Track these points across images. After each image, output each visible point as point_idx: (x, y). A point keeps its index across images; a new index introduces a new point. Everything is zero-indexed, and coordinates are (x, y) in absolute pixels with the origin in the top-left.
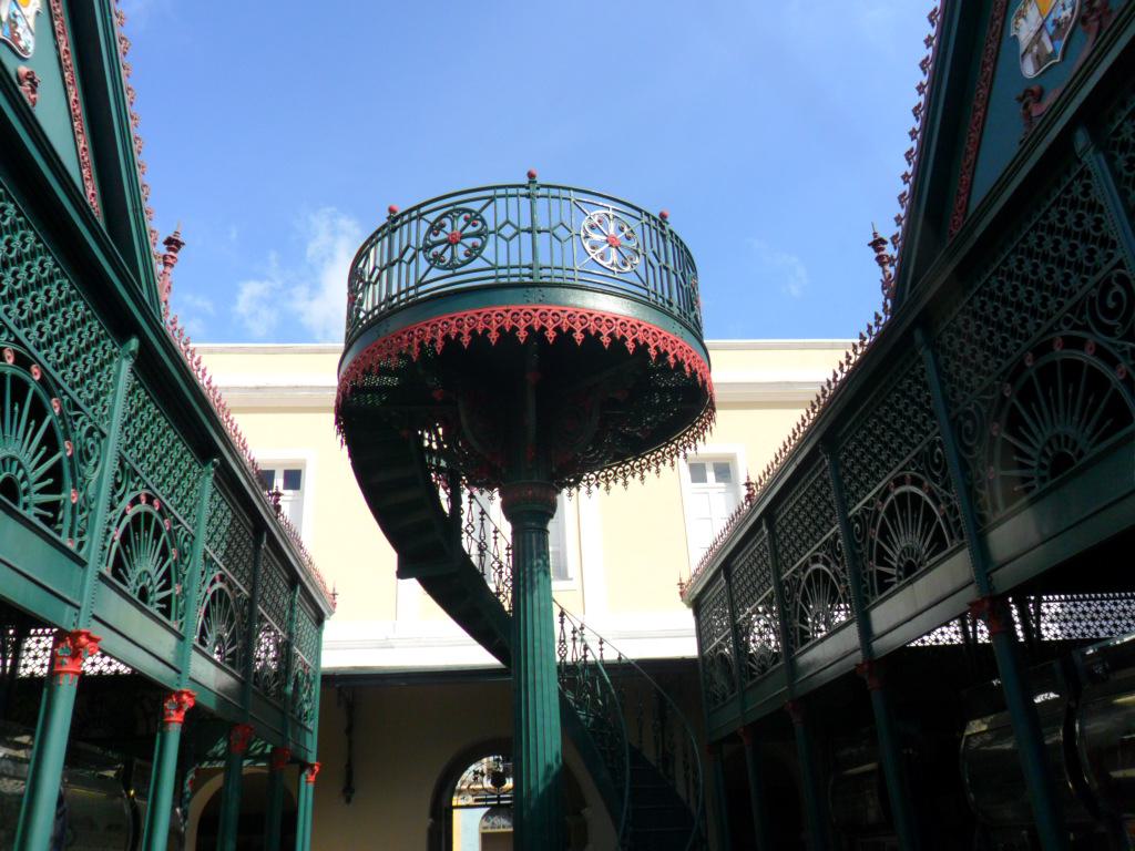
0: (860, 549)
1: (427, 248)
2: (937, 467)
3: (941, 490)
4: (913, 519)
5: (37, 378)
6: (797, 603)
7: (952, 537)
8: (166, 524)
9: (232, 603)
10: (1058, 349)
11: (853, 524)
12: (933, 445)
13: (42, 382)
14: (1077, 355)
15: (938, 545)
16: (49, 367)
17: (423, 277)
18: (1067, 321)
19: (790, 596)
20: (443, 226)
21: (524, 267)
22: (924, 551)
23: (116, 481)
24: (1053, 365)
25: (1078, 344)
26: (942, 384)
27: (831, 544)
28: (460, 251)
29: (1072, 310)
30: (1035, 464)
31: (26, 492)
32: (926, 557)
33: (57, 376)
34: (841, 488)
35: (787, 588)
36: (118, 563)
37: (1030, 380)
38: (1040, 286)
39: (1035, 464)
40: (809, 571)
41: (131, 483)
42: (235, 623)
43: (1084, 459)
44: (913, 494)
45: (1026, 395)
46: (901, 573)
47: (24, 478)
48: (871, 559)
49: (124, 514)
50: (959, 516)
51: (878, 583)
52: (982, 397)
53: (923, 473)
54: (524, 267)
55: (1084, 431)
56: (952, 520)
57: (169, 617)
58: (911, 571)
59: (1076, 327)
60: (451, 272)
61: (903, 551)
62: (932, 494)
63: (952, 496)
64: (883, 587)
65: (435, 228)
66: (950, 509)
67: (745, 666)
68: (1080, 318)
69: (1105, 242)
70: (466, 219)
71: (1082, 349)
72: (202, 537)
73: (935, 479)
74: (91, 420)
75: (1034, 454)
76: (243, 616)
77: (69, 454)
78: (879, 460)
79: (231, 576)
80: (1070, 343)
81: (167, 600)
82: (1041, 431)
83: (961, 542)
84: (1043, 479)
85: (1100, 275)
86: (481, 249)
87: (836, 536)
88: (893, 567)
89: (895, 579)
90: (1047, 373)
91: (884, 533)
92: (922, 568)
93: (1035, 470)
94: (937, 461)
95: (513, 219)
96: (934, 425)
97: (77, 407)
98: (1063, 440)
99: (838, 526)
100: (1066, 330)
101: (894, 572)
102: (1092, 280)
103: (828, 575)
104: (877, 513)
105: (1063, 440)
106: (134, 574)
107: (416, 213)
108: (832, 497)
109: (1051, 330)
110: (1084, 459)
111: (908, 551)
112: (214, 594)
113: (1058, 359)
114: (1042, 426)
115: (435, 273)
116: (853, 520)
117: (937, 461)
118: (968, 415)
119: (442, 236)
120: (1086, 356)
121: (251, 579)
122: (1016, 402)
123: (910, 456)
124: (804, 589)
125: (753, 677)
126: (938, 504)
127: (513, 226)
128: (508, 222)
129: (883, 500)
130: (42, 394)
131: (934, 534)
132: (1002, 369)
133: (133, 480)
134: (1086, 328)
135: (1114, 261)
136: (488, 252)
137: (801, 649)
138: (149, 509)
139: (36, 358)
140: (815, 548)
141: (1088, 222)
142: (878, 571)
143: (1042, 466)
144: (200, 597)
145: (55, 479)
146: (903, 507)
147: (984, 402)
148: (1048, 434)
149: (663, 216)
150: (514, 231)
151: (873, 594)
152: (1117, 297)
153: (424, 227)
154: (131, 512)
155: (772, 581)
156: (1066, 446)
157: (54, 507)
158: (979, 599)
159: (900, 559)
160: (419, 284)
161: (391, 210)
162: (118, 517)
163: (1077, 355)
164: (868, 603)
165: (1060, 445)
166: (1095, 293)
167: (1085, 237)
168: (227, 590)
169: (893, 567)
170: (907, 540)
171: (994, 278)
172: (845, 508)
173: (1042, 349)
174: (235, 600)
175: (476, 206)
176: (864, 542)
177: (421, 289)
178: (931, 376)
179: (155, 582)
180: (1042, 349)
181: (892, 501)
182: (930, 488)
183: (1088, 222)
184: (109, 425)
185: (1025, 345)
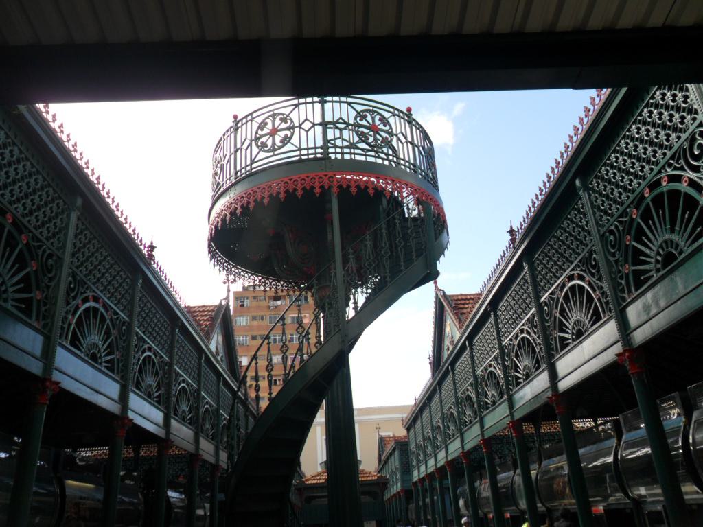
0: (548, 323)
1: (257, 139)
2: (594, 267)
3: (597, 282)
4: (580, 301)
5: (10, 221)
6: (555, 317)
7: (604, 312)
9: (157, 364)
10: (664, 184)
11: (543, 307)
12: (591, 253)
13: (14, 223)
14: (675, 186)
15: (596, 318)
16: (18, 215)
17: (255, 157)
18: (670, 165)
19: (550, 313)
20: (266, 124)
21: (318, 148)
22: (587, 322)
23: (70, 287)
24: (662, 194)
25: (678, 179)
26: (594, 213)
27: (531, 321)
28: (278, 139)
29: (672, 157)
30: (652, 260)
32: (590, 325)
33: (25, 221)
35: (546, 308)
37: (648, 205)
38: (651, 144)
39: (652, 260)
40: (519, 339)
41: (81, 288)
42: (160, 377)
43: (683, 255)
44: (579, 285)
45: (646, 216)
46: (574, 337)
48: (555, 329)
49: (77, 308)
50: (608, 298)
51: (560, 344)
52: (621, 219)
53: (584, 271)
54: (318, 148)
55: (683, 235)
58: (580, 335)
59: (676, 169)
60: (272, 154)
61: (575, 323)
62: (590, 285)
63: (603, 285)
64: (564, 346)
65: (262, 126)
67: (483, 402)
68: (677, 163)
69: (691, 111)
70: (267, 146)
71: (680, 182)
73: (593, 275)
74: (49, 249)
75: (652, 254)
76: (165, 373)
77: (34, 269)
78: (558, 265)
79: (155, 347)
82: (656, 239)
83: (611, 315)
84: (658, 270)
85: (687, 134)
86: (291, 138)
87: (533, 315)
88: (568, 333)
89: (570, 341)
91: (563, 312)
92: (587, 333)
93: (654, 264)
94: (594, 263)
95: (310, 118)
96: (591, 240)
97: (39, 240)
98: (669, 243)
99: (534, 310)
100: (669, 171)
101: (570, 336)
102: (684, 136)
103: (583, 287)
104: (558, 299)
105: (669, 243)
108: (530, 290)
109: (660, 172)
110: (683, 255)
111: (577, 322)
112: (144, 359)
113: (665, 189)
114: (657, 236)
115: (262, 155)
116: (543, 305)
117: (594, 263)
118: (611, 232)
120: (683, 186)
121: (170, 336)
122: (639, 220)
123: (584, 252)
124: (562, 304)
125: (488, 408)
126: (594, 291)
127: (310, 122)
128: (306, 120)
129: (561, 290)
130: (15, 233)
131: (593, 312)
132: (631, 199)
133: (83, 287)
134: (682, 169)
135: (697, 123)
136: (295, 140)
137: (517, 389)
139: (9, 209)
140: (521, 324)
142: (559, 336)
143: (657, 262)
146: (574, 295)
147: (621, 222)
148: (660, 240)
149: (409, 110)
150: (311, 125)
151: (557, 351)
153: (255, 125)
155: (497, 346)
156: (672, 248)
157: (28, 302)
158: (622, 351)
159: (573, 328)
160: (253, 162)
162: (72, 310)
163: (675, 186)
164: (554, 357)
165: (667, 248)
166: (686, 145)
167: (678, 109)
168: (153, 357)
169: (568, 333)
170: (578, 315)
171: (634, 126)
172: (538, 297)
173: (655, 184)
174: (159, 363)
176: (550, 318)
177: (254, 166)
178: (588, 209)
179: (102, 350)
180: (655, 184)
181: (567, 291)
182: (589, 282)
184: (64, 253)
185: (644, 183)
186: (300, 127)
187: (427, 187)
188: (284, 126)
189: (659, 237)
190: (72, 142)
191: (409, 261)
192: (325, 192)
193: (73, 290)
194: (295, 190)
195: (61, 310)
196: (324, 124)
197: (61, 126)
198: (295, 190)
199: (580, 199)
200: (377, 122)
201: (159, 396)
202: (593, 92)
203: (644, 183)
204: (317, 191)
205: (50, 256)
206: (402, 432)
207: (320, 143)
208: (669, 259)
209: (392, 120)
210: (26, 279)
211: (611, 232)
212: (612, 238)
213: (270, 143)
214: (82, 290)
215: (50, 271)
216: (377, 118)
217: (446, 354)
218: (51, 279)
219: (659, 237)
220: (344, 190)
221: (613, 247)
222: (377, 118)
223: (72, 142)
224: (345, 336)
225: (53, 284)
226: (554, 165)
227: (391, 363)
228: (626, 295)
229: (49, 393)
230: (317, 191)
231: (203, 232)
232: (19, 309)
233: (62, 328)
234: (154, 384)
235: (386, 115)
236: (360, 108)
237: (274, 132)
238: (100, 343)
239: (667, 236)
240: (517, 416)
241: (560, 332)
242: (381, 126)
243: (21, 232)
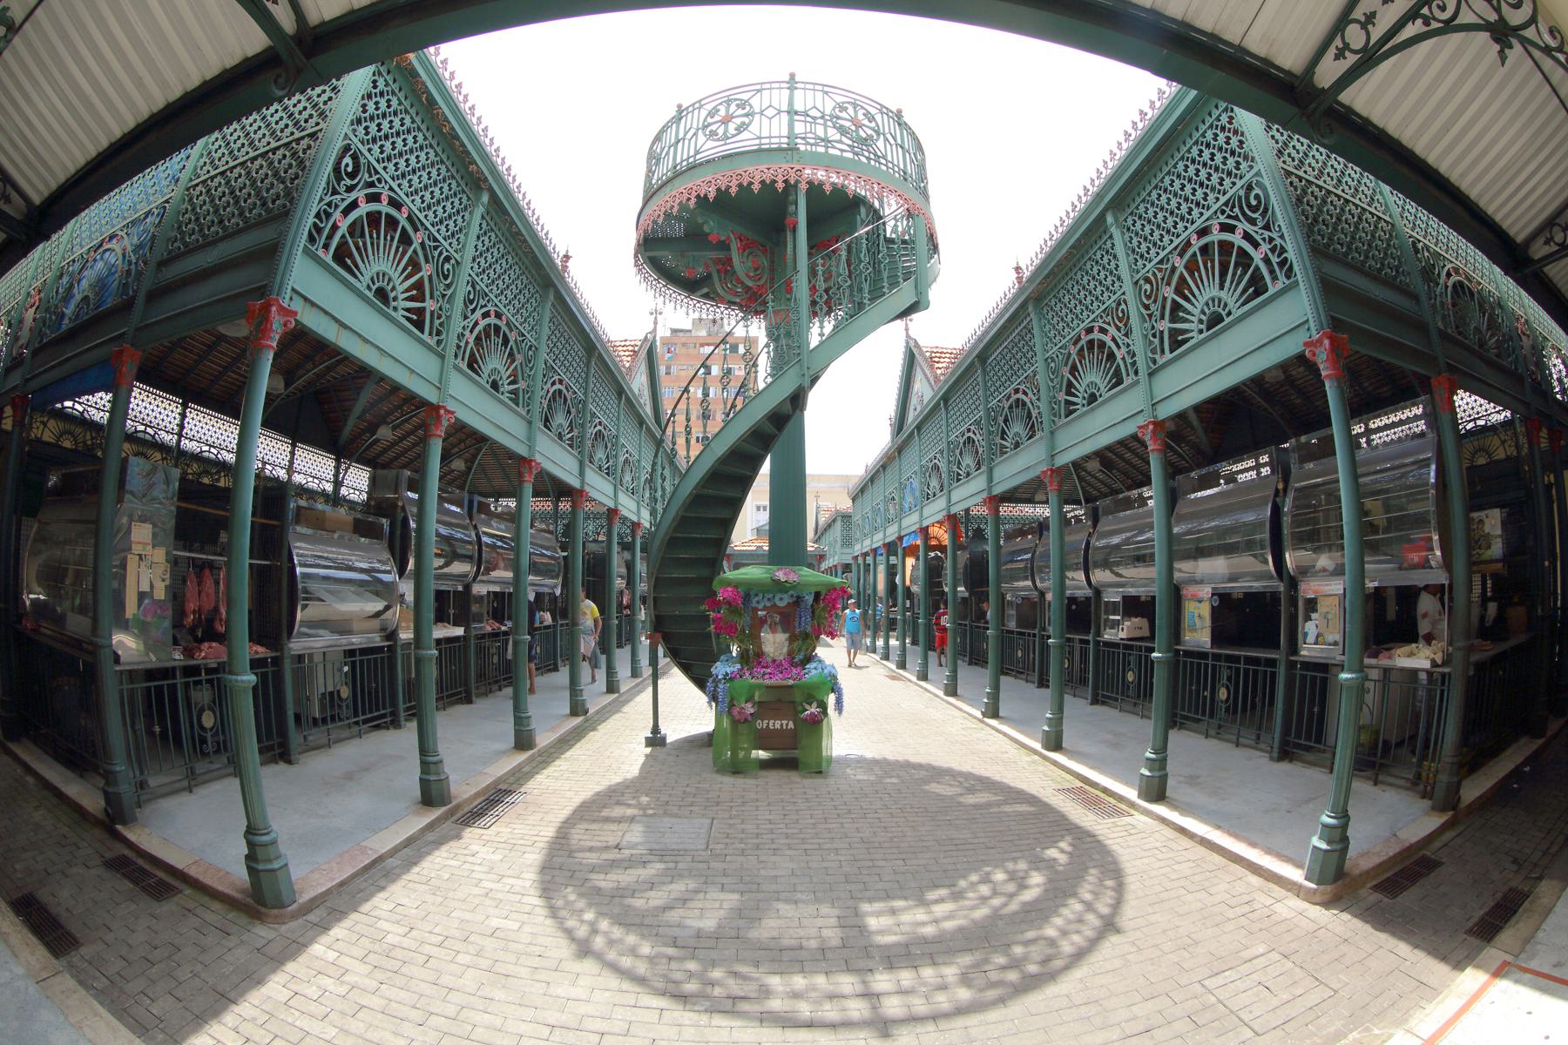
8: (512, 337)
18: (1223, 212)
19: (995, 419)
25: (1230, 229)
27: (977, 423)
28: (732, 128)
29: (1226, 204)
31: (395, 299)
33: (421, 216)
34: (986, 389)
36: (547, 420)
47: (394, 288)
49: (476, 324)
56: (1129, 361)
57: (421, 328)
59: (1229, 217)
65: (711, 114)
66: (1273, 250)
72: (544, 349)
73: (1119, 329)
80: (1226, 228)
81: (515, 392)
84: (1201, 332)
90: (1091, 343)
91: (1074, 369)
97: (435, 240)
102: (1239, 183)
106: (554, 424)
107: (698, 105)
111: (1017, 434)
115: (710, 144)
118: (1147, 280)
119: (717, 118)
134: (1236, 218)
136: (754, 128)
138: (497, 322)
141: (1234, 141)
144: (543, 393)
145: (418, 292)
149: (899, 111)
152: (1257, 197)
153: (704, 113)
154: (483, 323)
160: (697, 153)
161: (679, 106)
163: (1226, 236)
166: (1242, 193)
175: (745, 97)
180: (1203, 232)
183: (1234, 141)
186: (761, 113)
187: (915, 197)
188: (740, 112)
189: (1208, 292)
190: (469, 104)
191: (894, 284)
192: (790, 188)
193: (471, 302)
194: (751, 183)
195: (457, 324)
196: (792, 112)
197: (445, 62)
198: (751, 183)
199: (1111, 237)
200: (861, 117)
201: (571, 439)
202: (1162, 83)
203: (1191, 228)
204: (780, 186)
205: (447, 259)
206: (845, 504)
207: (785, 132)
208: (1215, 320)
209: (878, 118)
210: (419, 285)
211: (1147, 280)
212: (1148, 287)
213: (721, 131)
214: (482, 302)
215: (446, 277)
216: (861, 112)
217: (911, 416)
218: (448, 286)
219: (1208, 292)
220: (815, 189)
221: (1148, 297)
222: (861, 112)
223: (469, 104)
224: (799, 372)
225: (449, 292)
226: (1082, 193)
227: (850, 419)
228: (1157, 357)
229: (445, 423)
230: (780, 186)
231: (630, 238)
232: (408, 319)
233: (459, 347)
234: (566, 424)
235: (873, 111)
236: (840, 99)
237: (726, 121)
238: (503, 370)
239: (1215, 292)
240: (997, 490)
241: (1173, 320)
242: (866, 122)
243: (416, 230)
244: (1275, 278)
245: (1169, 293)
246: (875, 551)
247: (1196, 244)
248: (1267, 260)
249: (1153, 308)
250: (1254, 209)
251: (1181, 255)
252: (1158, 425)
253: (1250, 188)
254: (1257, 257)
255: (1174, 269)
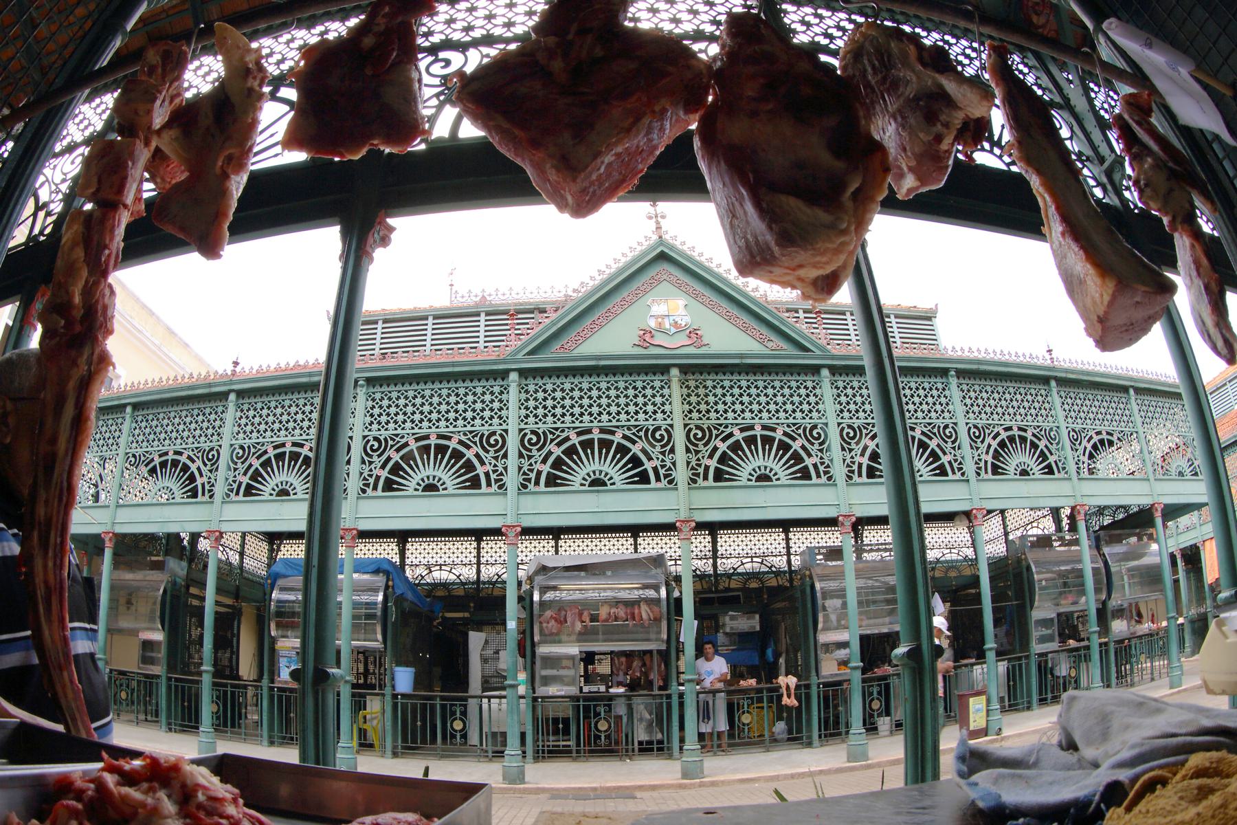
29: (471, 432)
134: (475, 443)
141: (218, 423)
183: (218, 423)
212: (241, 452)
244: (203, 494)
245: (256, 464)
246: (754, 114)
247: (171, 456)
248: (203, 485)
249: (239, 465)
250: (209, 460)
251: (160, 456)
252: (115, 535)
253: (212, 449)
254: (199, 481)
255: (153, 460)
